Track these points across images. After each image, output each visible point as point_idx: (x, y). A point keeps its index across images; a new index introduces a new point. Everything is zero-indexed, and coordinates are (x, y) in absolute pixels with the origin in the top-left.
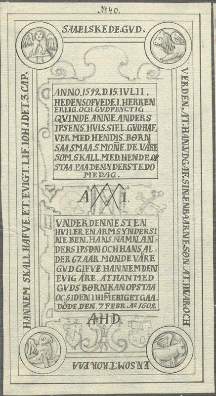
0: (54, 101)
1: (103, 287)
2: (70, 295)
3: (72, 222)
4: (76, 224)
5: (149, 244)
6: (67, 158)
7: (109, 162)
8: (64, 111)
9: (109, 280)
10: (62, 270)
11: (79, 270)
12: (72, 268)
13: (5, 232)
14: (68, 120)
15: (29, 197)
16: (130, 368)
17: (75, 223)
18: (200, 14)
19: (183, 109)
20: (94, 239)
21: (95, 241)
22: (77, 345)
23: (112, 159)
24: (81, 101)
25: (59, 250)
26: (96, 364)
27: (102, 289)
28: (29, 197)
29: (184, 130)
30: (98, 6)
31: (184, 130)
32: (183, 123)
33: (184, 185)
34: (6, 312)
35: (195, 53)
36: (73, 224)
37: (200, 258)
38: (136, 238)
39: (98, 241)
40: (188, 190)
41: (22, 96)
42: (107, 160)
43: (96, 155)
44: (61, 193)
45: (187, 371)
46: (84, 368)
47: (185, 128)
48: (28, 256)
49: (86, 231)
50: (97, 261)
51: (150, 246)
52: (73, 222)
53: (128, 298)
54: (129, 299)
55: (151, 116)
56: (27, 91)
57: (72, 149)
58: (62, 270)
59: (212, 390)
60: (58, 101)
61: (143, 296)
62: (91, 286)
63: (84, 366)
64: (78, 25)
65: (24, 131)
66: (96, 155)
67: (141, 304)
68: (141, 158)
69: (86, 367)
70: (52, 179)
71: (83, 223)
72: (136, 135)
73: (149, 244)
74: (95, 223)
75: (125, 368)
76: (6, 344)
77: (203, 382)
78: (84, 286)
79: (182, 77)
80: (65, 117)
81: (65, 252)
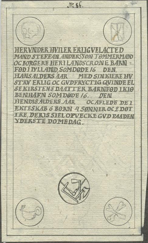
0: (15, 49)
1: (103, 89)
6: (68, 70)
7: (84, 79)
9: (121, 88)
10: (66, 83)
12: (50, 121)
14: (111, 83)
20: (18, 76)
21: (19, 77)
22: (79, 77)
26: (64, 77)
27: (103, 90)
38: (125, 62)
39: (65, 103)
42: (83, 78)
43: (68, 61)
53: (36, 64)
54: (37, 64)
55: (60, 100)
57: (33, 57)
62: (60, 108)
66: (68, 61)
68: (83, 70)
69: (115, 115)
72: (62, 107)
78: (56, 107)
80: (110, 81)
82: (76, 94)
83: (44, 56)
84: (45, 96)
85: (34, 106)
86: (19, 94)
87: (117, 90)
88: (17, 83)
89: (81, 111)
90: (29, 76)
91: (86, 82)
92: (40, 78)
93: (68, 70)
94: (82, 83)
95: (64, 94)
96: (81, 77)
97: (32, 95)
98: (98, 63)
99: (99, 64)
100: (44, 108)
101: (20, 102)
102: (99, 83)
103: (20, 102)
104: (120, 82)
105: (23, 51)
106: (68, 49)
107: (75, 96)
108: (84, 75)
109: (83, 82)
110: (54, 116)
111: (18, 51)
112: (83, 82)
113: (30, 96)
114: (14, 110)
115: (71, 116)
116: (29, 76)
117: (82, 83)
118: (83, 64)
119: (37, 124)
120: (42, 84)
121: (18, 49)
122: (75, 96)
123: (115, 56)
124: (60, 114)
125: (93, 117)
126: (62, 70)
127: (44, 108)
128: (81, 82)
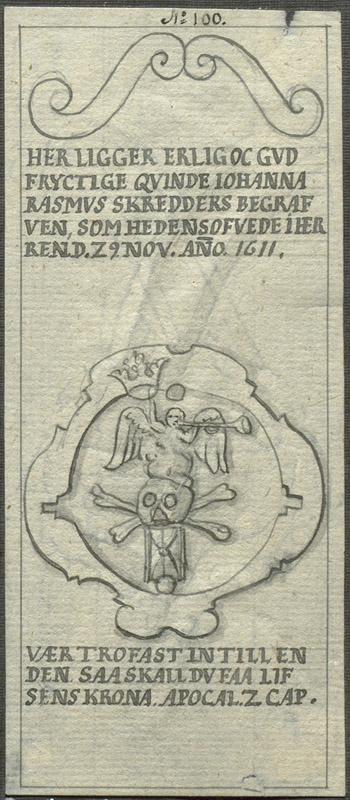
2: (206, 221)
3: (189, 178)
4: (236, 181)
8: (190, 161)
16: (211, 222)
17: (196, 180)
23: (50, 161)
24: (195, 224)
25: (268, 227)
36: (193, 183)
39: (113, 679)
44: (269, 588)
49: (167, 154)
50: (67, 165)
52: (192, 178)
54: (129, 161)
59: (339, 788)
60: (35, 154)
61: (108, 179)
67: (242, 243)
70: (304, 498)
71: (59, 159)
81: (56, 162)
82: (201, 175)
84: (65, 680)
85: (121, 197)
86: (249, 202)
87: (295, 158)
88: (162, 656)
90: (69, 698)
91: (65, 181)
94: (51, 185)
97: (247, 181)
98: (122, 698)
99: (124, 700)
104: (189, 201)
105: (141, 159)
109: (55, 181)
111: (39, 160)
112: (55, 181)
113: (243, 184)
114: (24, 254)
116: (69, 698)
117: (51, 185)
120: (80, 165)
121: (39, 154)
123: (254, 226)
124: (46, 246)
126: (89, 676)
128: (49, 180)
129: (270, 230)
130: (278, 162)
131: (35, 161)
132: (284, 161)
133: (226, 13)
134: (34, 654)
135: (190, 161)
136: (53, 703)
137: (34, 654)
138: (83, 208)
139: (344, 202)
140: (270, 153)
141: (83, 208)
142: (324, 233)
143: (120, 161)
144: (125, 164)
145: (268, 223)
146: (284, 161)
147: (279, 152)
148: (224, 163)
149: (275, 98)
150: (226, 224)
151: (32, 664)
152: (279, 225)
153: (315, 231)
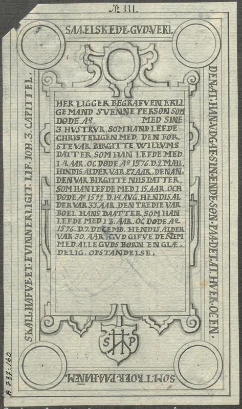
5: (177, 193)
8: (168, 32)
11: (124, 104)
13: (7, 307)
15: (31, 89)
18: (228, 13)
19: (211, 260)
28: (31, 89)
29: (211, 106)
30: (110, 6)
31: (211, 106)
32: (211, 98)
33: (211, 162)
34: (7, 176)
35: (223, 55)
37: (226, 33)
40: (217, 168)
41: (25, 134)
45: (218, 26)
46: (111, 380)
47: (213, 104)
48: (30, 80)
51: (178, 195)
55: (178, 143)
56: (31, 127)
58: (137, 31)
59: (235, 400)
63: (110, 379)
64: (98, 383)
65: (27, 146)
73: (177, 193)
74: (213, 73)
75: (154, 212)
76: (7, 176)
77: (230, 395)
79: (211, 292)
83: (100, 188)
86: (95, 179)
89: (100, 212)
92: (94, 174)
93: (70, 113)
95: (148, 178)
96: (87, 222)
100: (82, 205)
101: (63, 104)
102: (102, 245)
103: (63, 104)
106: (123, 380)
107: (113, 164)
108: (92, 220)
110: (29, 337)
115: (95, 254)
118: (115, 245)
119: (208, 130)
122: (113, 164)
125: (109, 31)
127: (82, 205)
129: (98, 173)
130: (139, 33)
131: (212, 280)
132: (142, 31)
133: (137, 5)
134: (153, 29)
135: (146, 206)
136: (117, 114)
137: (153, 29)
138: (212, 284)
139: (238, 78)
140: (136, 28)
141: (212, 284)
142: (183, 247)
143: (124, 104)
144: (132, 239)
145: (214, 194)
146: (142, 31)
147: (27, 288)
148: (135, 33)
149: (130, 57)
150: (215, 250)
151: (59, 240)
152: (168, 102)
153: (211, 298)
